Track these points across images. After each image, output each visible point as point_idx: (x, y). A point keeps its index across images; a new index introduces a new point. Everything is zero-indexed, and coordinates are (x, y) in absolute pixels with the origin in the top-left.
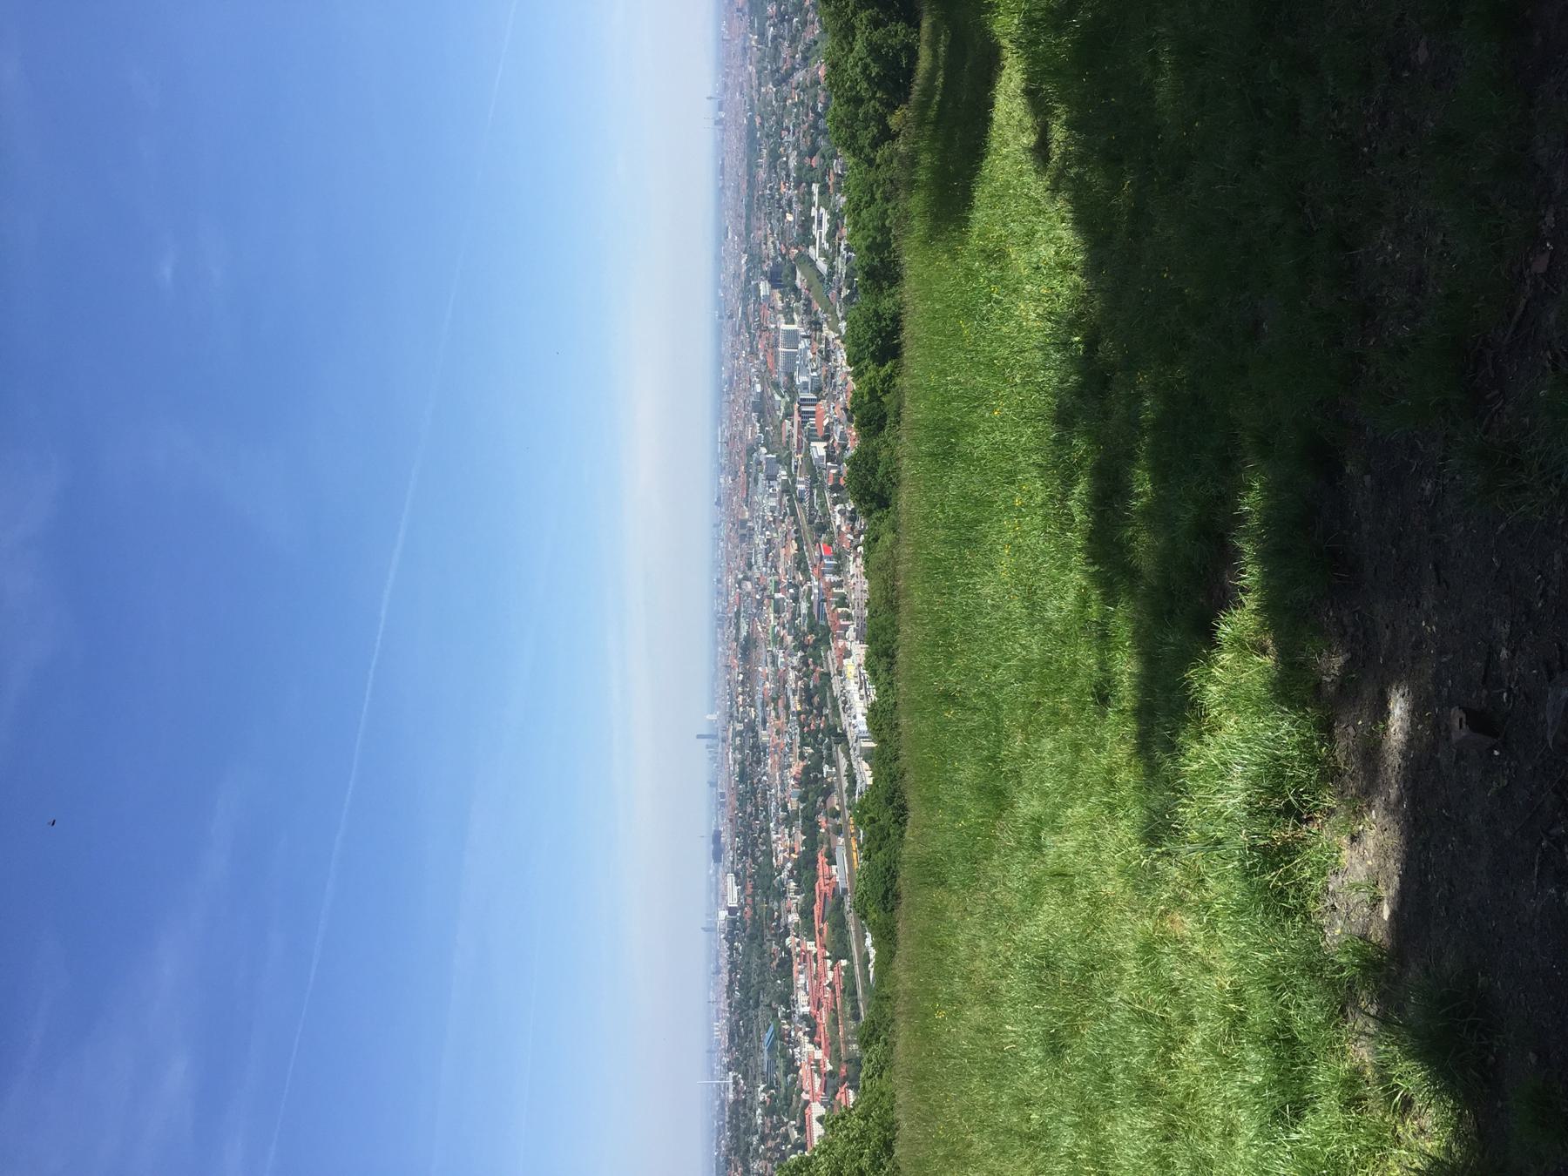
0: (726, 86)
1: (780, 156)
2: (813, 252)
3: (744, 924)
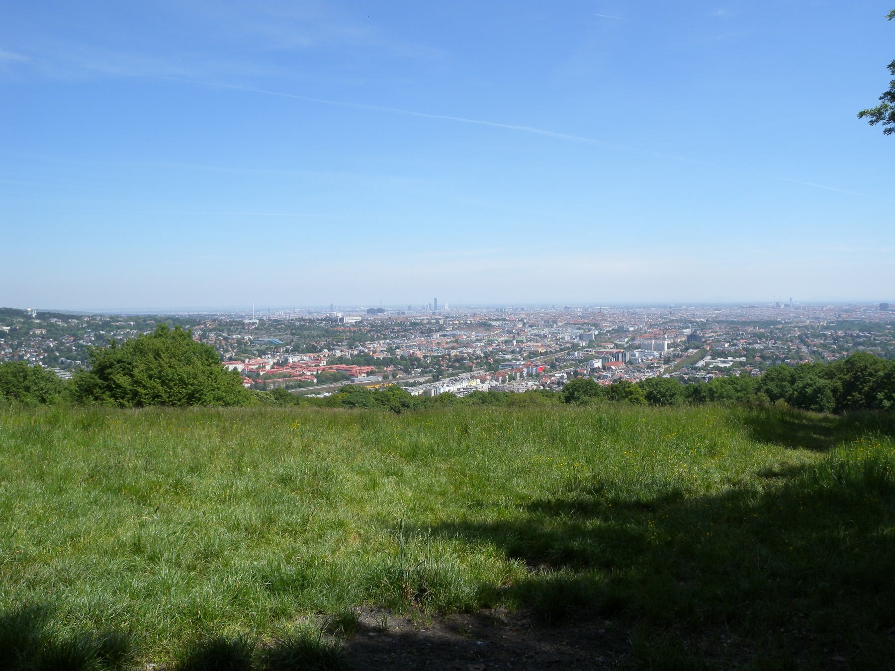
0: (797, 308)
1: (760, 339)
2: (708, 358)
3: (335, 326)
